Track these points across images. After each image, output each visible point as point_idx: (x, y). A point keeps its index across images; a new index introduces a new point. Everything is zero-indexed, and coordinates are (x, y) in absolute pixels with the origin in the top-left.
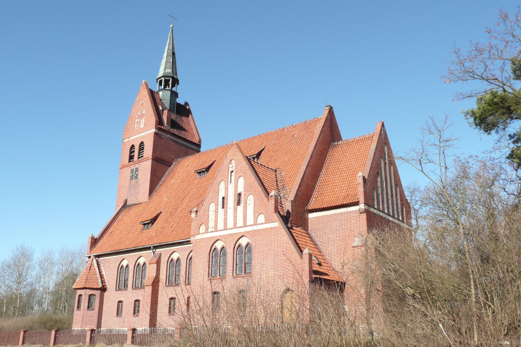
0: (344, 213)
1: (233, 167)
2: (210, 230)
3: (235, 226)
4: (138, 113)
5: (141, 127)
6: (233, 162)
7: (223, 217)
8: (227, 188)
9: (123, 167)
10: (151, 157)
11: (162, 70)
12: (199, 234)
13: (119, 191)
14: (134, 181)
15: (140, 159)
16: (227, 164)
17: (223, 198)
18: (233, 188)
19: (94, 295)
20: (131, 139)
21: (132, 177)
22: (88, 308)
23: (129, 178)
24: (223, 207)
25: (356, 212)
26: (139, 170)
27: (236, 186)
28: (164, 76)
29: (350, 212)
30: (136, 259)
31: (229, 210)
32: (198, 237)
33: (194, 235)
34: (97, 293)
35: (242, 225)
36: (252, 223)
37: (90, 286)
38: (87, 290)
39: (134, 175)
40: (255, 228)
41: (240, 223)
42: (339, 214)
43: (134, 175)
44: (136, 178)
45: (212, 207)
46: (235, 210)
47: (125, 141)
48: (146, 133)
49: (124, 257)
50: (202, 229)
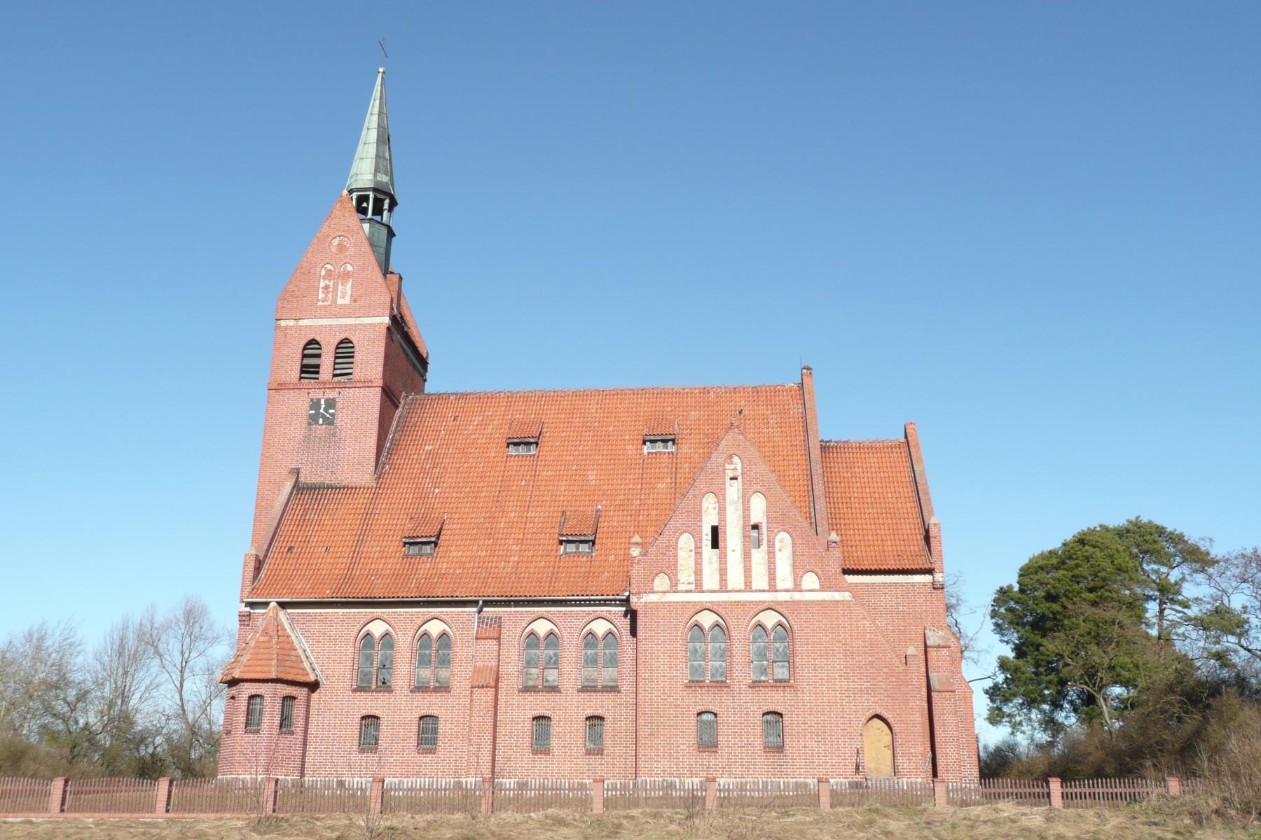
0: (902, 585)
1: (735, 469)
2: (681, 587)
3: (748, 588)
4: (329, 267)
5: (340, 301)
6: (736, 459)
7: (716, 565)
8: (722, 511)
9: (281, 387)
10: (380, 383)
11: (364, 173)
12: (652, 592)
13: (266, 444)
14: (321, 429)
15: (336, 379)
16: (721, 461)
17: (715, 530)
18: (740, 513)
19: (294, 698)
20: (301, 323)
21: (313, 419)
22: (247, 724)
23: (305, 419)
24: (715, 544)
25: (925, 584)
26: (339, 405)
27: (746, 510)
28: (375, 190)
29: (913, 584)
30: (419, 622)
31: (730, 555)
32: (652, 598)
33: (639, 593)
34: (301, 693)
35: (767, 588)
36: (790, 586)
37: (290, 677)
38: (279, 686)
39: (322, 415)
40: (797, 596)
41: (760, 580)
42: (891, 584)
43: (322, 415)
44: (330, 422)
45: (686, 541)
46: (747, 557)
47: (283, 323)
48: (359, 321)
49: (375, 615)
50: (661, 582)
